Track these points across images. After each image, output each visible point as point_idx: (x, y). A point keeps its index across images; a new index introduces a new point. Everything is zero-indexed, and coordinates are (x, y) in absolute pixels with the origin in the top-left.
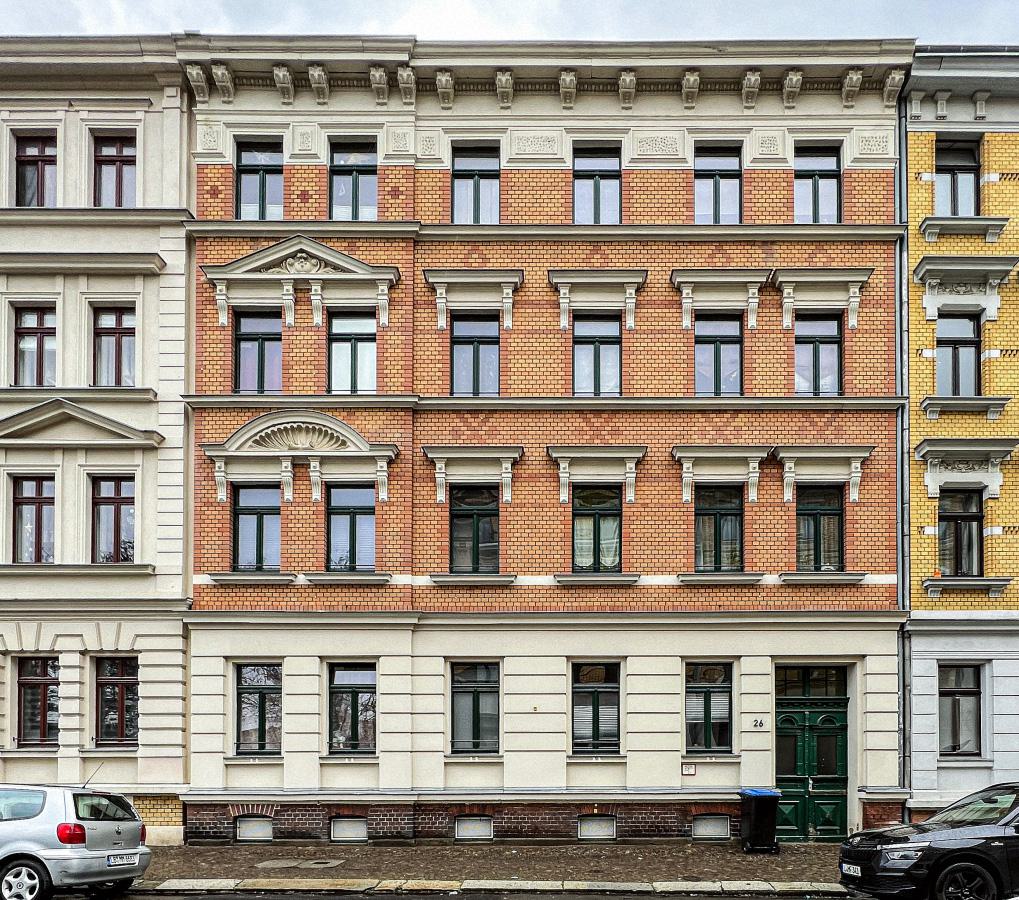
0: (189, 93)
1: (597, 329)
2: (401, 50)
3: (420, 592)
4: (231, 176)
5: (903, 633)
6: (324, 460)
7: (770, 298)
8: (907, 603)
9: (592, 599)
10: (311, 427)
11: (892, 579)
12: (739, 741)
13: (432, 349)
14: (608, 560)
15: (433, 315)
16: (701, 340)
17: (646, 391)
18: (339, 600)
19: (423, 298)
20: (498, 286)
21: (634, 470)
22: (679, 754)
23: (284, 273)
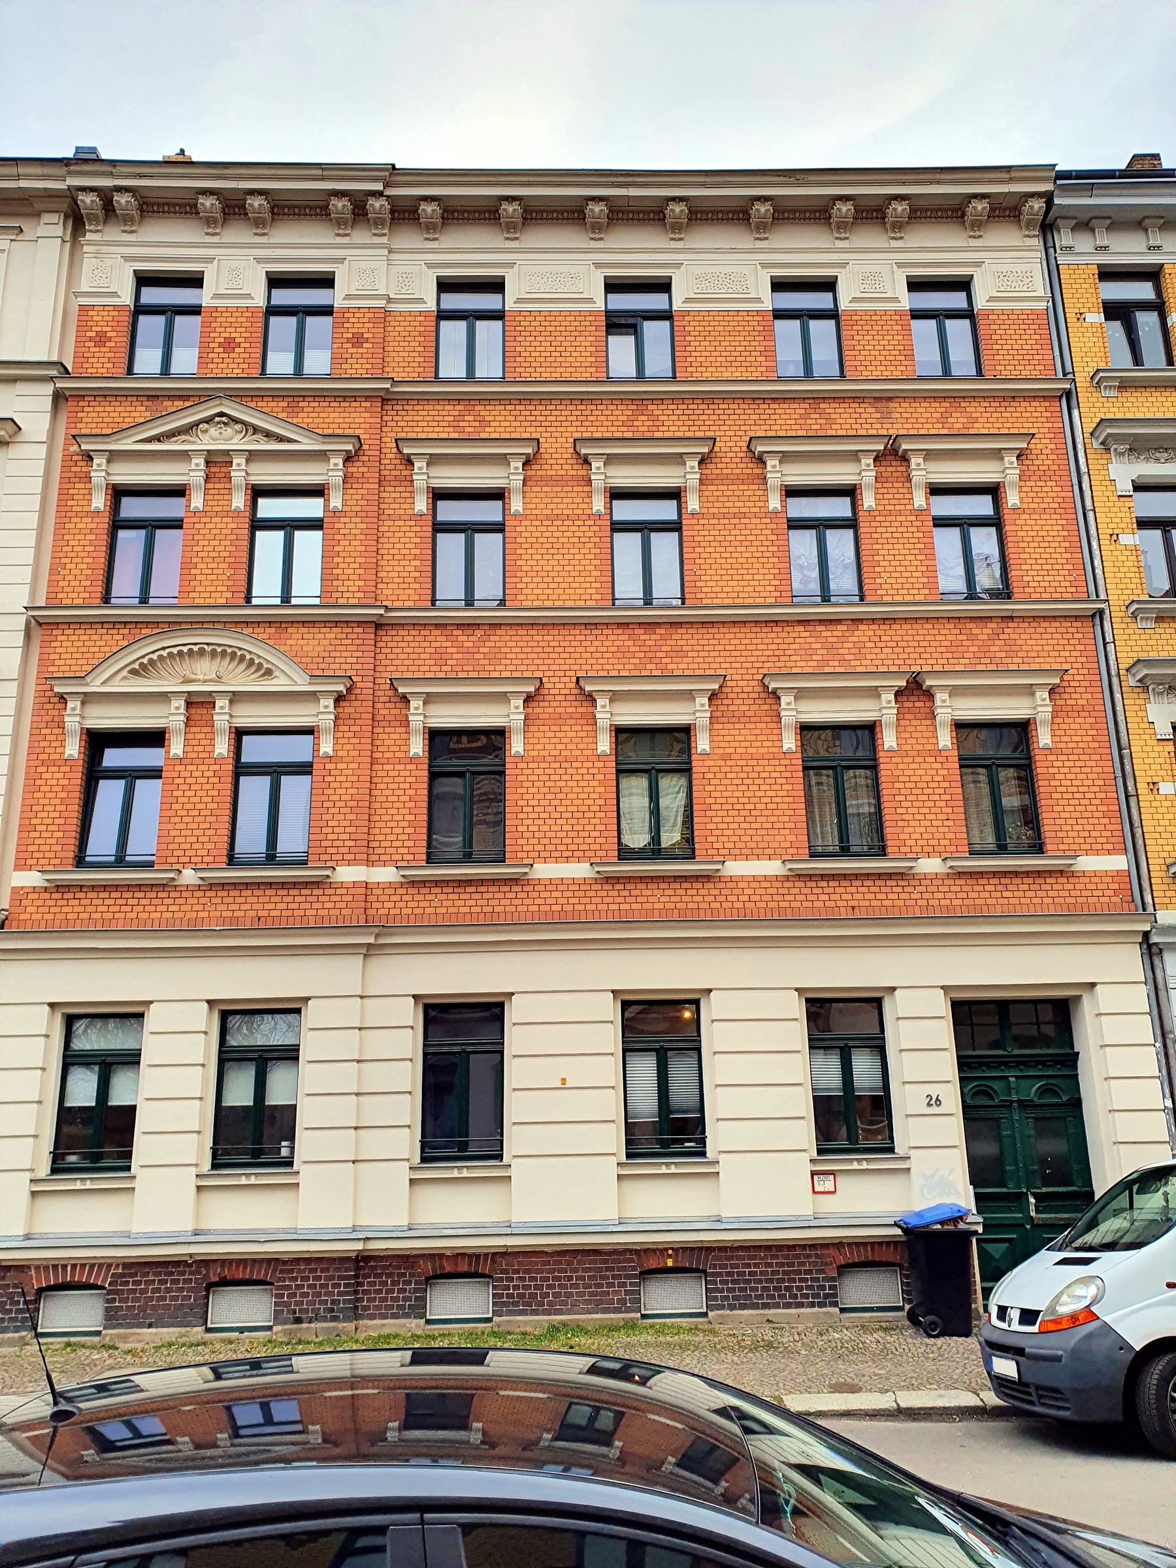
0: (77, 221)
1: (652, 516)
2: (375, 179)
3: (380, 892)
4: (126, 319)
5: (1150, 946)
6: (236, 698)
7: (893, 469)
8: (1148, 899)
9: (651, 899)
10: (219, 650)
11: (1120, 862)
12: (905, 1132)
13: (404, 541)
14: (671, 837)
15: (408, 495)
16: (796, 524)
17: (719, 595)
18: (248, 906)
19: (393, 473)
20: (503, 459)
21: (707, 708)
22: (806, 1157)
23: (194, 443)
